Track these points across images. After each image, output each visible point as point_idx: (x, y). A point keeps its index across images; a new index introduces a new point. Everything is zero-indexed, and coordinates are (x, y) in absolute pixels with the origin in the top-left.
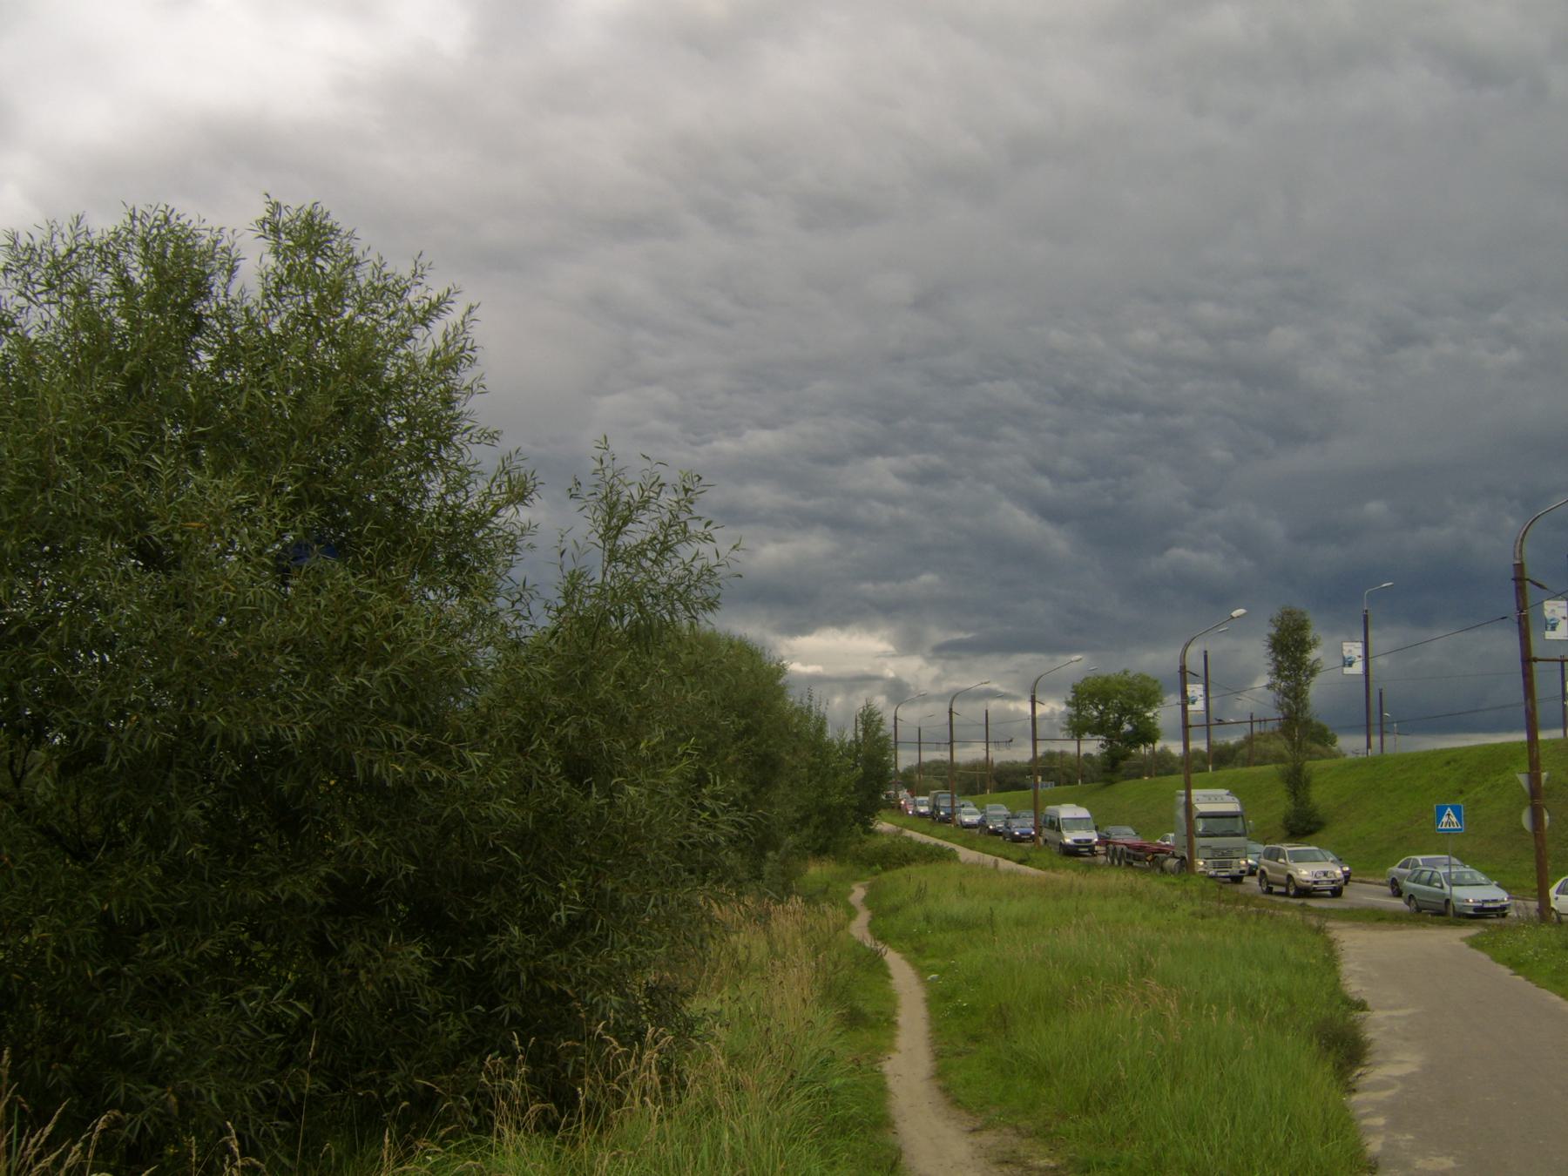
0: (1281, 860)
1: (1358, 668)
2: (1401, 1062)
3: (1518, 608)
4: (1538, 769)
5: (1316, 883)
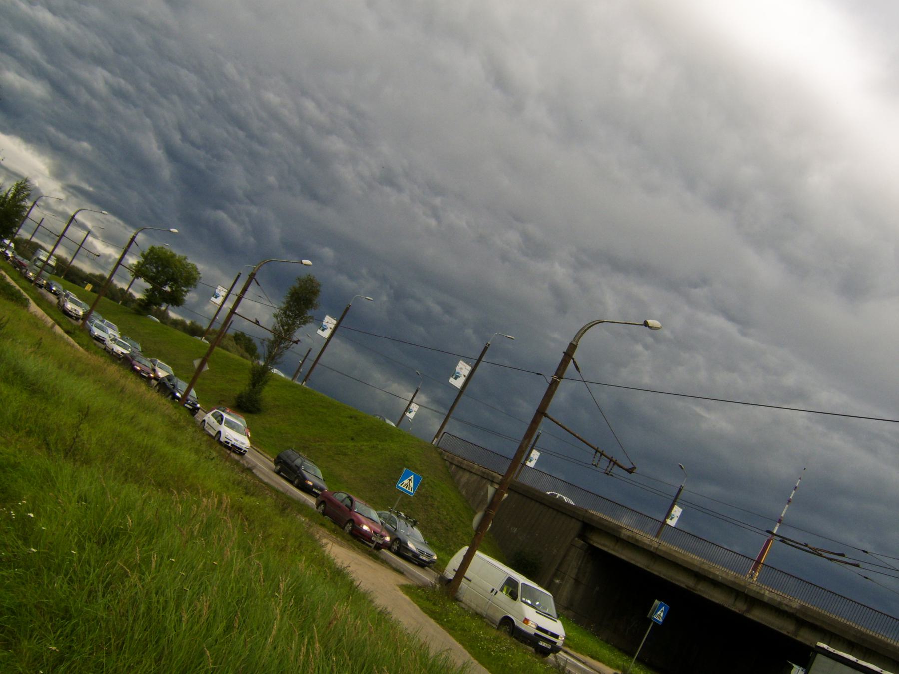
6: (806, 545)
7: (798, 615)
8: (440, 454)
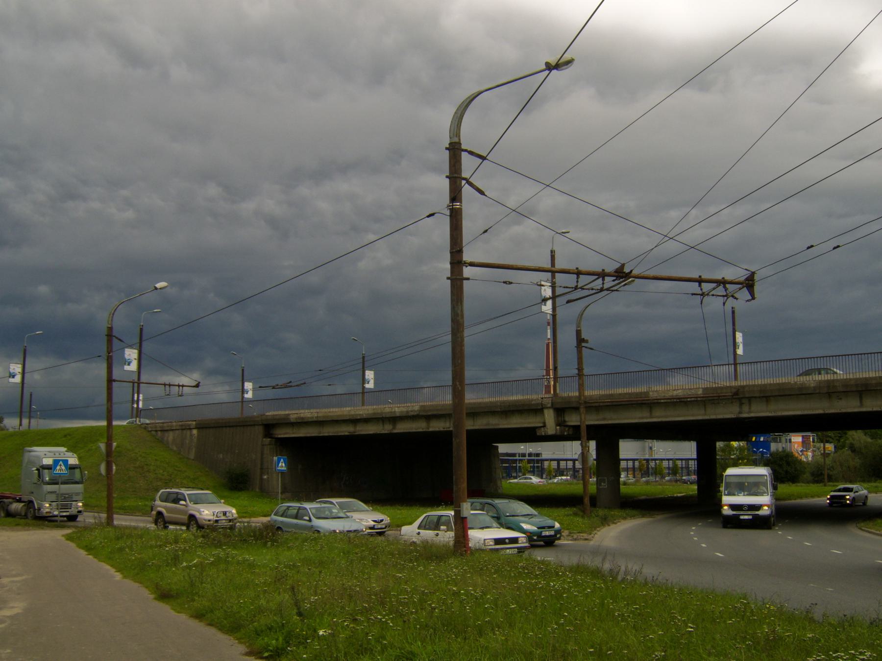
0: (183, 502)
1: (18, 379)
2: (13, 607)
3: (108, 352)
4: (111, 441)
5: (217, 521)
6: (277, 385)
7: (421, 414)
8: (145, 428)
